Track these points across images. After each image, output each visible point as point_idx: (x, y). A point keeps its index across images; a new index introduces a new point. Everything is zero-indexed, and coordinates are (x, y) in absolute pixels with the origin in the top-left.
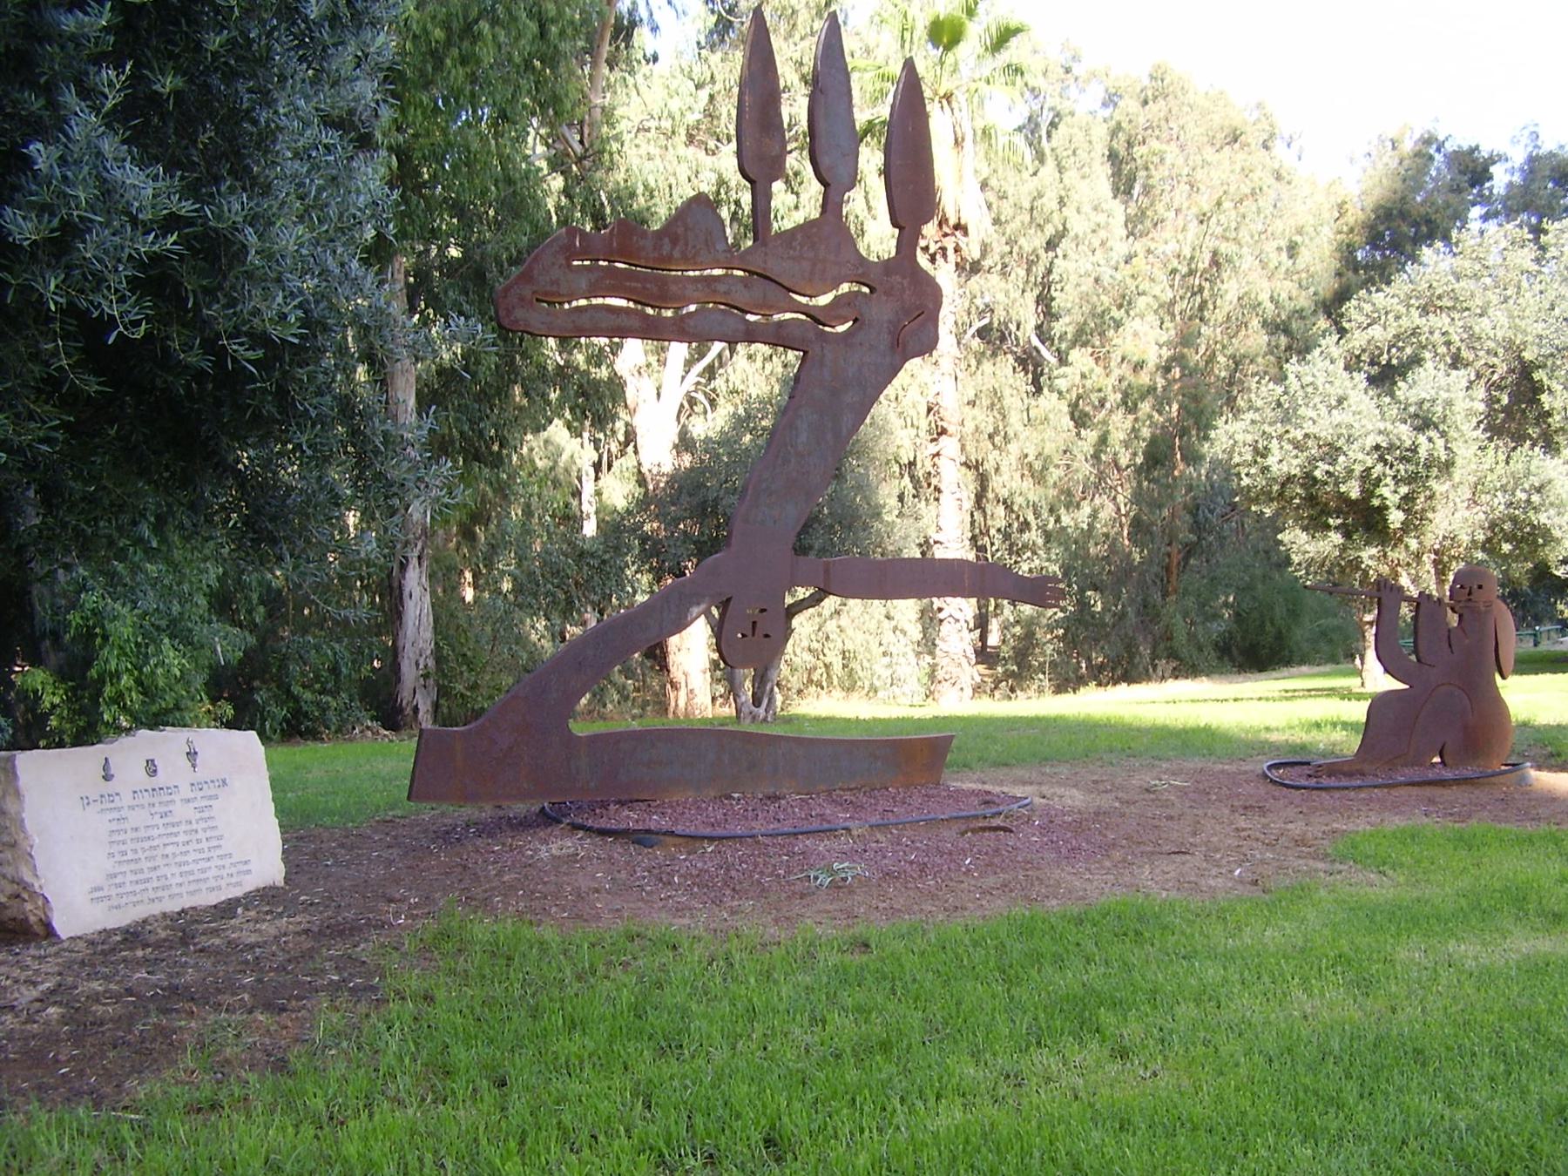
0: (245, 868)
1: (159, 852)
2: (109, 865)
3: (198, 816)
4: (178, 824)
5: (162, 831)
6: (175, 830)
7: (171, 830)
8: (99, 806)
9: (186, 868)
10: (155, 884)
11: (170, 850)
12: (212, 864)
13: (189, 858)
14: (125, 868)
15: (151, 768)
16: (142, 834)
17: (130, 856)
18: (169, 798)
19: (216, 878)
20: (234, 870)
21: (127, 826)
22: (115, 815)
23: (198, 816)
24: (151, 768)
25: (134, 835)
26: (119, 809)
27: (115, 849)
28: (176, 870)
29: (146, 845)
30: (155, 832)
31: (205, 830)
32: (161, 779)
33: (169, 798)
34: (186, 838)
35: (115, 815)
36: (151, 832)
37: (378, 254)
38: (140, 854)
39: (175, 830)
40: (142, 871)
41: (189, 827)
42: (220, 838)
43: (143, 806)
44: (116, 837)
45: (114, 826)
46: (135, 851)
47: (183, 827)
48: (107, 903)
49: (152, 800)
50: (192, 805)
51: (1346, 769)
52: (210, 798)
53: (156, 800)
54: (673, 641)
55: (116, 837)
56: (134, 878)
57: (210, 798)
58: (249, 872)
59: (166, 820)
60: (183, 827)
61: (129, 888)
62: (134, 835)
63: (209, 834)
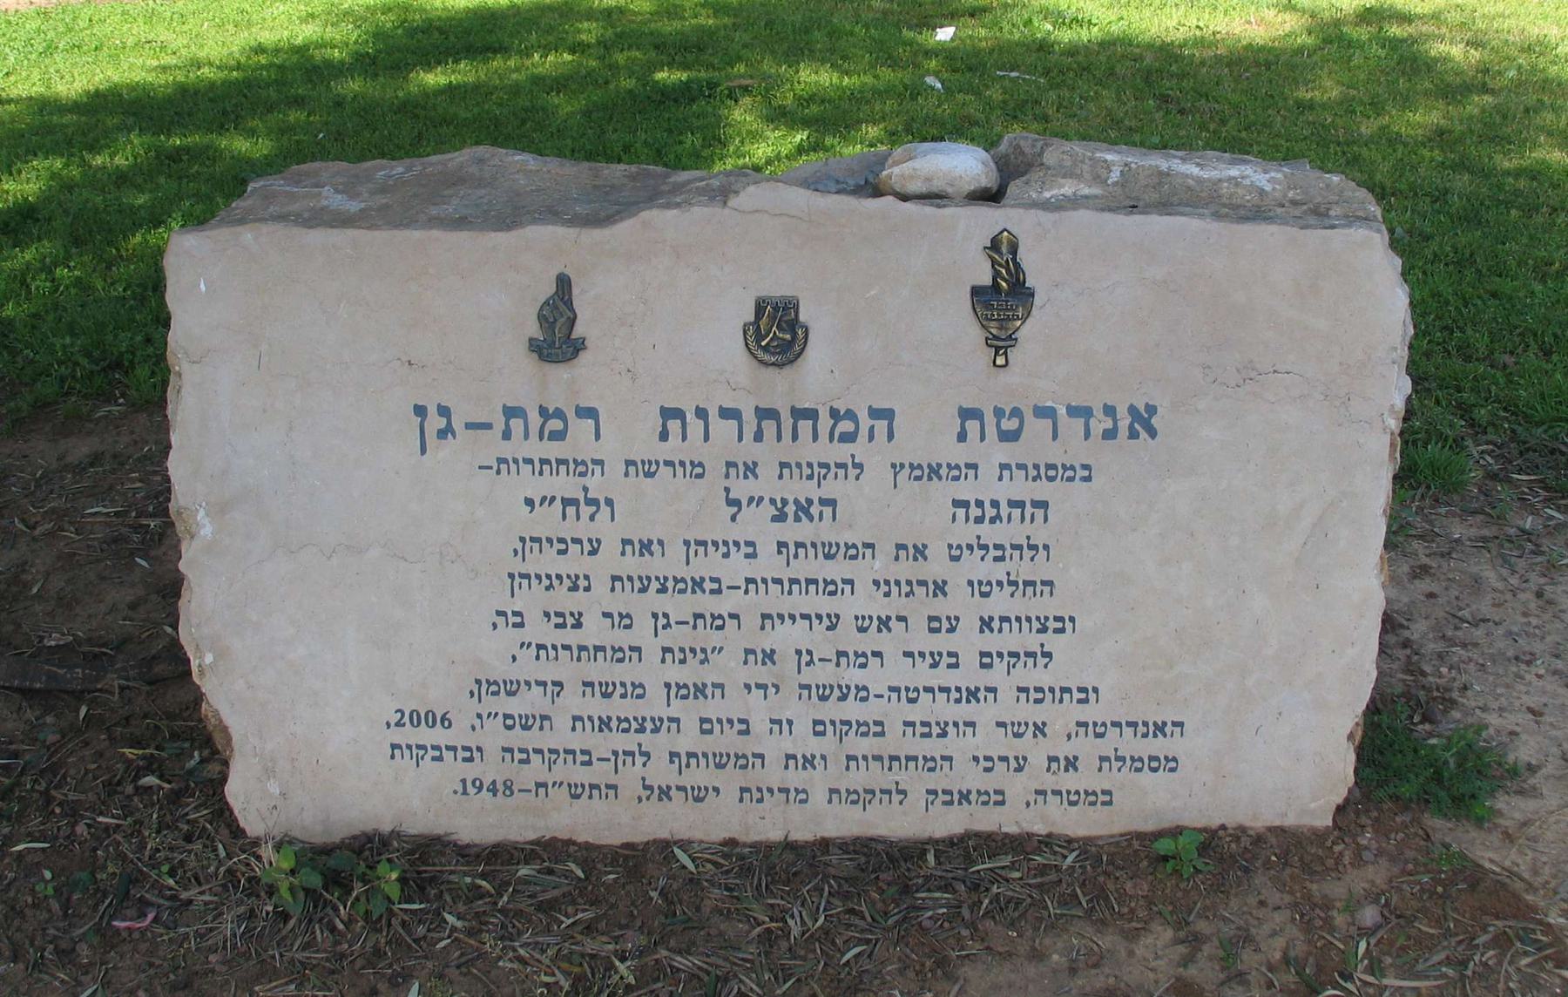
0: (1158, 746)
1: (733, 640)
2: (496, 652)
3: (966, 533)
4: (852, 552)
5: (769, 564)
6: (836, 570)
7: (804, 567)
8: (491, 446)
9: (852, 710)
10: (684, 744)
11: (786, 637)
12: (986, 713)
13: (876, 677)
14: (564, 669)
15: (777, 332)
16: (669, 564)
17: (595, 631)
18: (842, 452)
19: (988, 763)
20: (1086, 747)
21: (606, 529)
22: (564, 484)
23: (966, 533)
24: (777, 332)
25: (632, 564)
26: (581, 468)
27: (531, 600)
28: (802, 712)
29: (679, 606)
30: (735, 568)
31: (983, 590)
32: (817, 376)
33: (842, 452)
34: (878, 606)
35: (564, 484)
36: (706, 565)
37: (1234, 91)
38: (642, 633)
39: (836, 570)
40: (638, 690)
41: (906, 569)
42: (1062, 624)
43: (697, 469)
44: (546, 562)
45: (548, 522)
46: (626, 621)
47: (880, 565)
48: (454, 769)
49: (749, 450)
50: (943, 492)
51: (521, 167)
52: (1049, 472)
53: (767, 454)
54: (1398, 262)
55: (546, 562)
56: (596, 707)
57: (1049, 472)
58: (1171, 763)
59: (793, 531)
60: (880, 565)
61: (561, 735)
62: (632, 564)
63: (1000, 603)
